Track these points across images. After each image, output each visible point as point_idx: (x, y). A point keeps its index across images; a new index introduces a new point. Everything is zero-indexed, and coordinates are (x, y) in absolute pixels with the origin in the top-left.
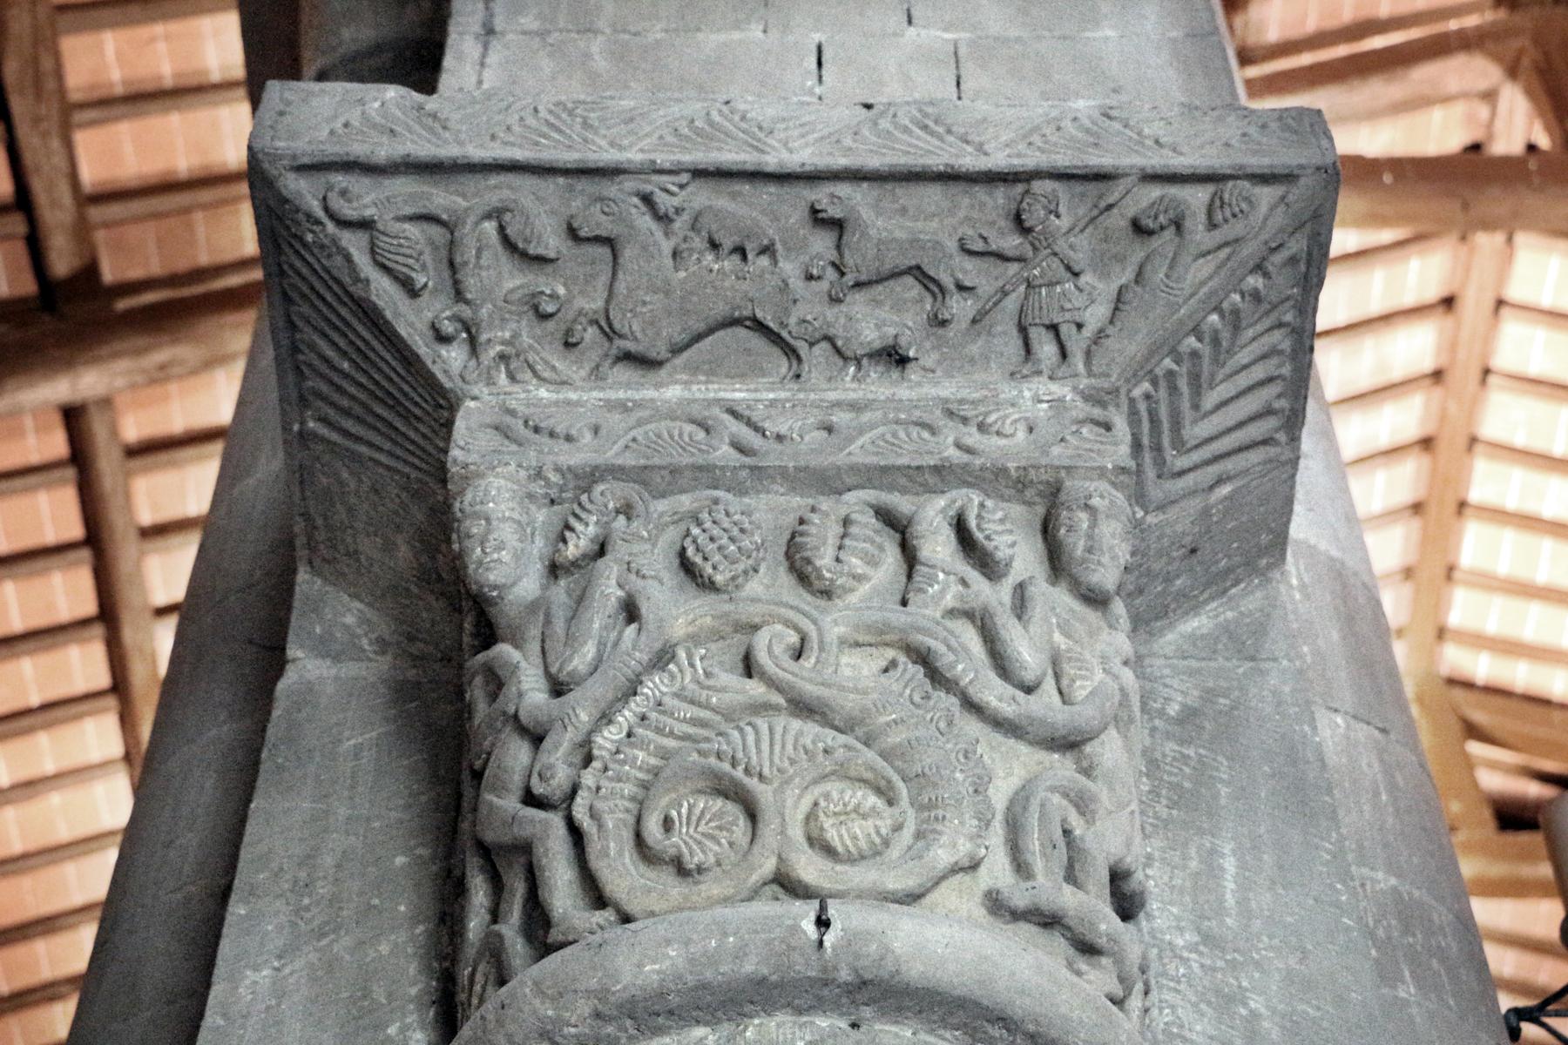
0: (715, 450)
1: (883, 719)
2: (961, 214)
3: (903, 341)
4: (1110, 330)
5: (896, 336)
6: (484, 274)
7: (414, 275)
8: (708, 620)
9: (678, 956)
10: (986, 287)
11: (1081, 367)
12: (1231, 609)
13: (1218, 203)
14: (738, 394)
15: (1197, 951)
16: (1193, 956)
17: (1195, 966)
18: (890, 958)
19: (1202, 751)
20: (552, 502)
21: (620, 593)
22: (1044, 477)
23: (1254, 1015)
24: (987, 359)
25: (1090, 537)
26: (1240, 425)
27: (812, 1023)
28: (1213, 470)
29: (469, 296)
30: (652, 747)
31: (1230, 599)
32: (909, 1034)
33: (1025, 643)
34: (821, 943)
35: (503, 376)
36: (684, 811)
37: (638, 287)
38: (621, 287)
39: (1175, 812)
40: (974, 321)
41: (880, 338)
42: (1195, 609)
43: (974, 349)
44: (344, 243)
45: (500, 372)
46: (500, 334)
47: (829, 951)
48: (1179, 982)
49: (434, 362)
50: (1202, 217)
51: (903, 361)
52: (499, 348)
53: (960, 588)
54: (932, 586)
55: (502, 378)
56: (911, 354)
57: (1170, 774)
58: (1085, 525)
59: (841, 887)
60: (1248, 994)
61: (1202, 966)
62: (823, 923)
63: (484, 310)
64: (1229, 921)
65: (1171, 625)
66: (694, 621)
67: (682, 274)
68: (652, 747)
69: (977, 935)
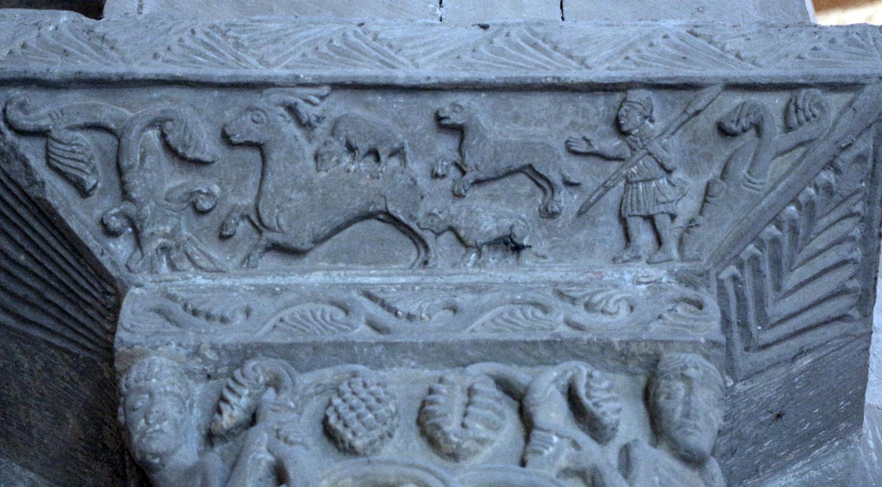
0: (353, 328)
2: (567, 120)
3: (517, 231)
4: (700, 220)
5: (511, 227)
6: (148, 176)
7: (85, 177)
11: (675, 254)
12: (815, 469)
13: (792, 108)
14: (373, 278)
20: (209, 377)
21: (270, 458)
22: (644, 350)
25: (687, 403)
29: (134, 195)
35: (165, 265)
37: (285, 186)
38: (269, 186)
40: (580, 214)
41: (498, 228)
43: (581, 237)
44: (21, 150)
45: (161, 261)
46: (161, 228)
49: (102, 254)
50: (779, 121)
51: (518, 249)
52: (160, 241)
53: (573, 450)
54: (547, 448)
55: (164, 268)
56: (525, 242)
58: (682, 393)
63: (148, 207)
67: (323, 174)
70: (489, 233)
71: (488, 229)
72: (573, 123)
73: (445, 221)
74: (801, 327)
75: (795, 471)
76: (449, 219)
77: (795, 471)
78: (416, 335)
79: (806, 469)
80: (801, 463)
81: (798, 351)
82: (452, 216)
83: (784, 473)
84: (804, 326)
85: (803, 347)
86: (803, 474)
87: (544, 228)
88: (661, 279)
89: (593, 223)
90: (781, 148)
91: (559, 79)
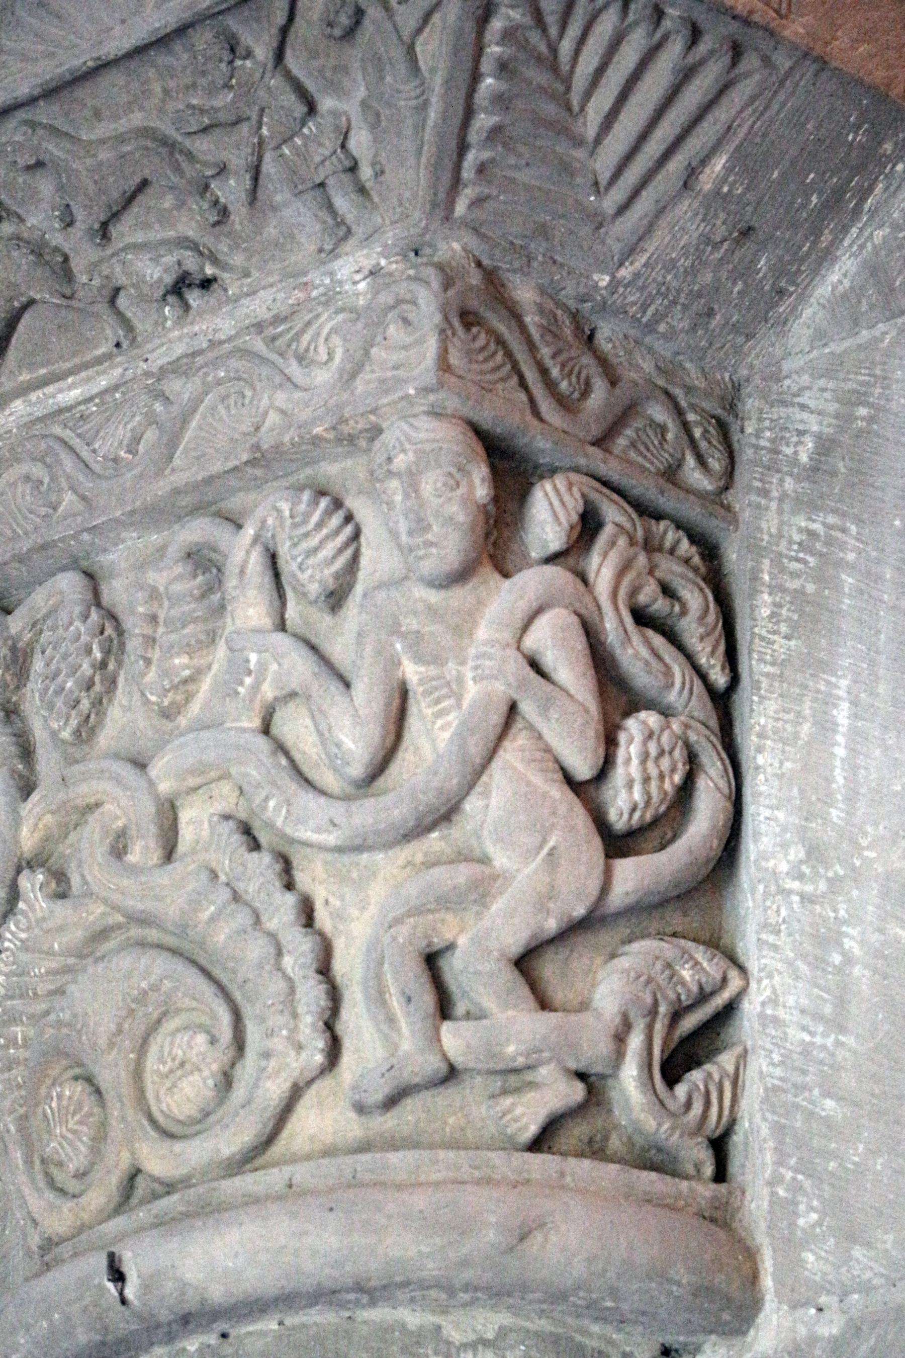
1: (205, 915)
2: (157, 88)
5: (179, 263)
8: (49, 818)
9: (27, 1342)
10: (239, 159)
12: (881, 226)
15: (801, 877)
16: (795, 885)
17: (796, 899)
18: (190, 1292)
19: (831, 519)
23: (849, 960)
24: (292, 236)
26: (643, 137)
27: (184, 1349)
28: (676, 165)
30: (24, 1019)
31: (873, 213)
32: (274, 1326)
33: (347, 722)
34: (123, 1301)
36: (54, 1104)
39: (793, 643)
41: (165, 271)
42: (827, 257)
43: (271, 231)
47: (136, 1302)
48: (778, 932)
57: (795, 575)
59: (185, 1171)
60: (844, 929)
61: (803, 896)
62: (118, 1276)
64: (834, 812)
65: (803, 298)
66: (36, 825)
68: (24, 1019)
69: (763, 788)
70: (160, 279)
71: (155, 277)
72: (166, 92)
73: (103, 286)
74: (671, 138)
75: (851, 246)
76: (105, 282)
77: (851, 246)
78: (129, 496)
79: (866, 234)
80: (854, 231)
81: (685, 174)
82: (107, 277)
83: (836, 259)
84: (677, 130)
85: (689, 164)
86: (862, 247)
87: (222, 238)
88: (378, 264)
89: (274, 208)
90: (352, 133)
91: (99, 58)
